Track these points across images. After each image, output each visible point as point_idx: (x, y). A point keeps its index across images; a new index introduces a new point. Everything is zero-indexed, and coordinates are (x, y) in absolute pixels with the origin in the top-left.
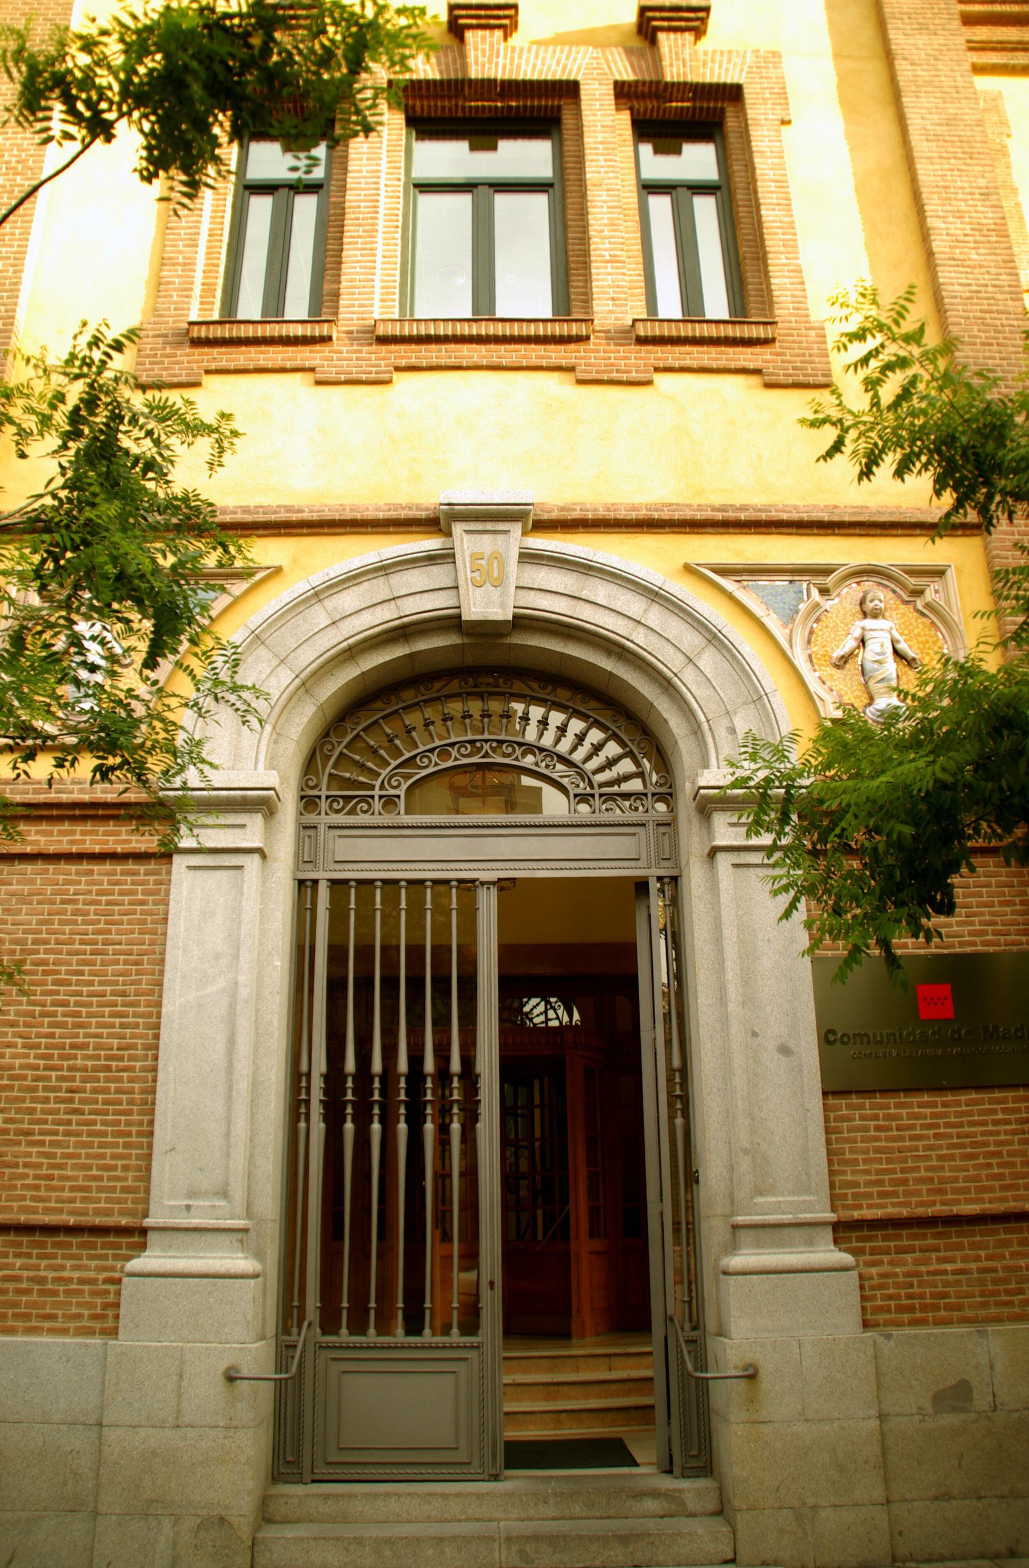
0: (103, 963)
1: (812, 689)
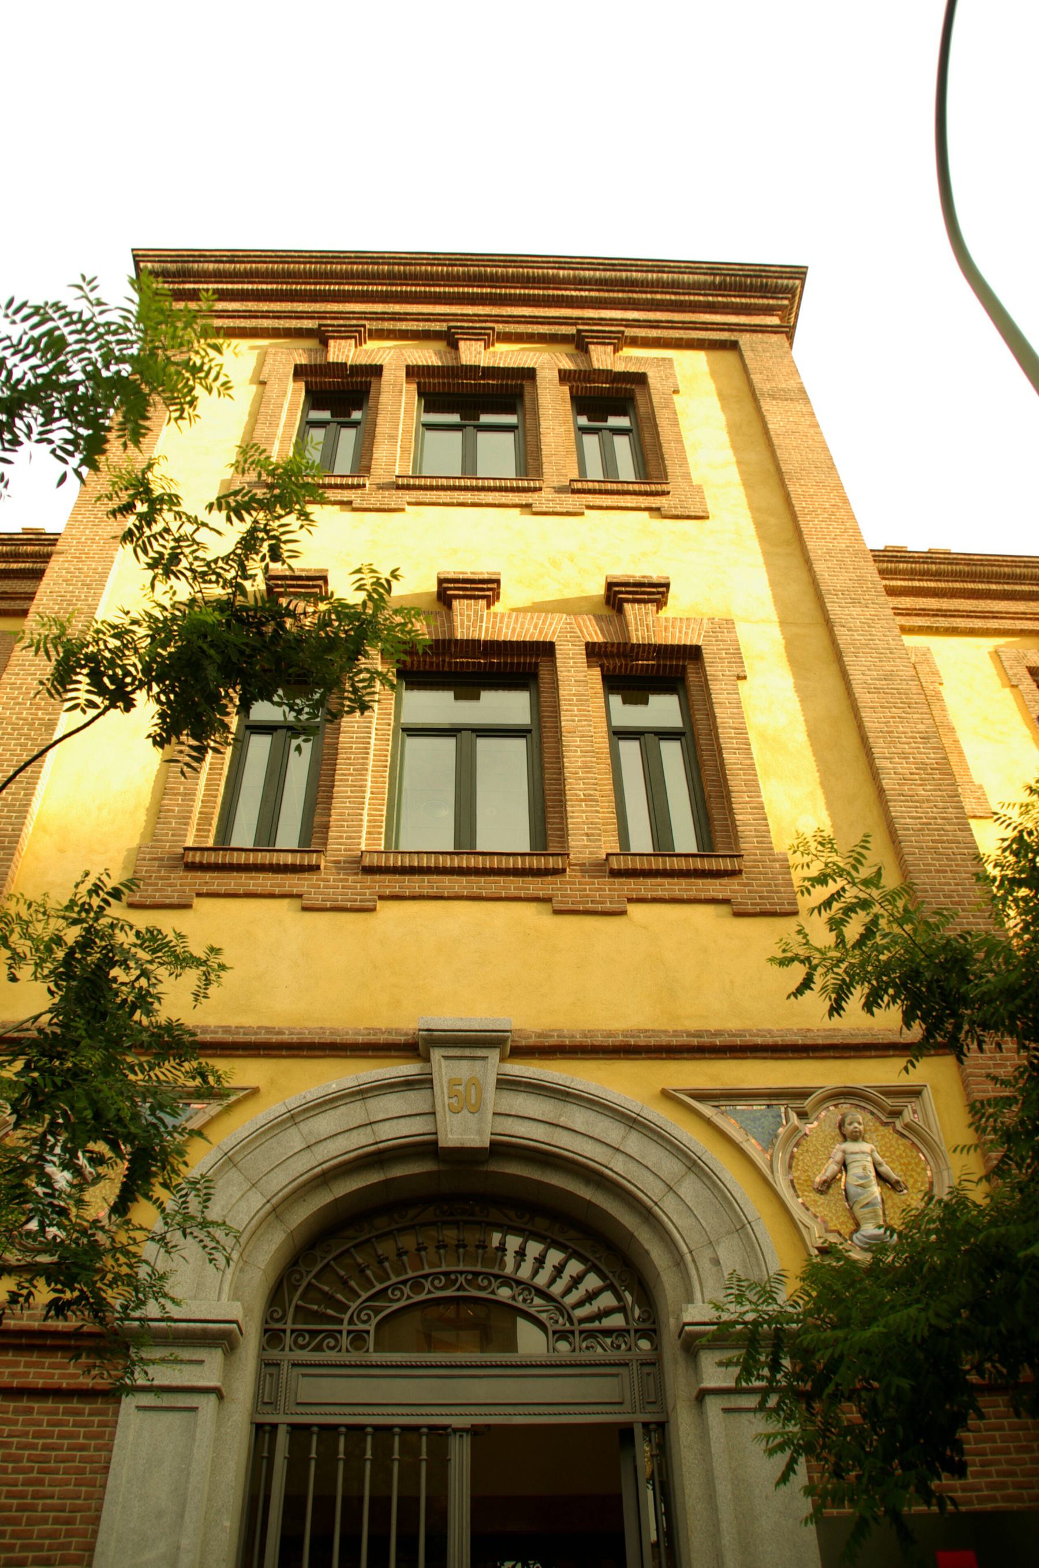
0: (30, 1522)
1: (796, 1217)
